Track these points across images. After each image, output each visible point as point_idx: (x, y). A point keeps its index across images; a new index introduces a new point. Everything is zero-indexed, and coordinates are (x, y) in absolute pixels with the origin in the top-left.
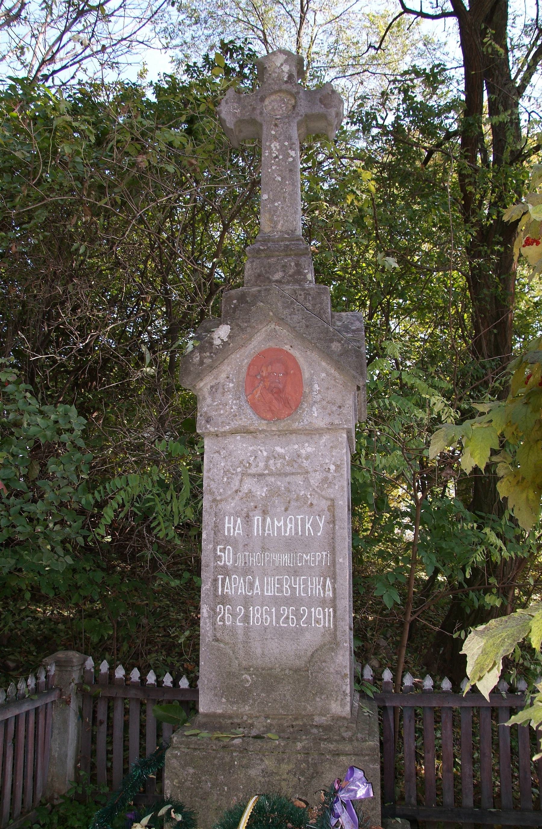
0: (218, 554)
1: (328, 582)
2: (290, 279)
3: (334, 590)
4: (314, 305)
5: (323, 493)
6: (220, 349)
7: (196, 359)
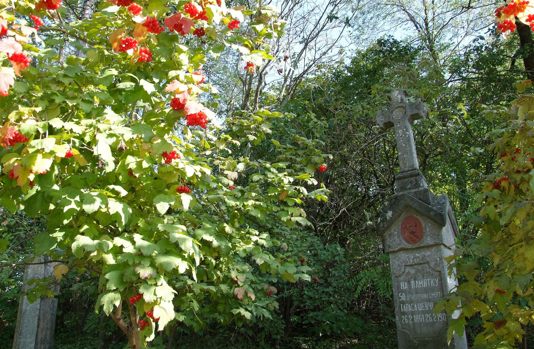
4: (424, 197)
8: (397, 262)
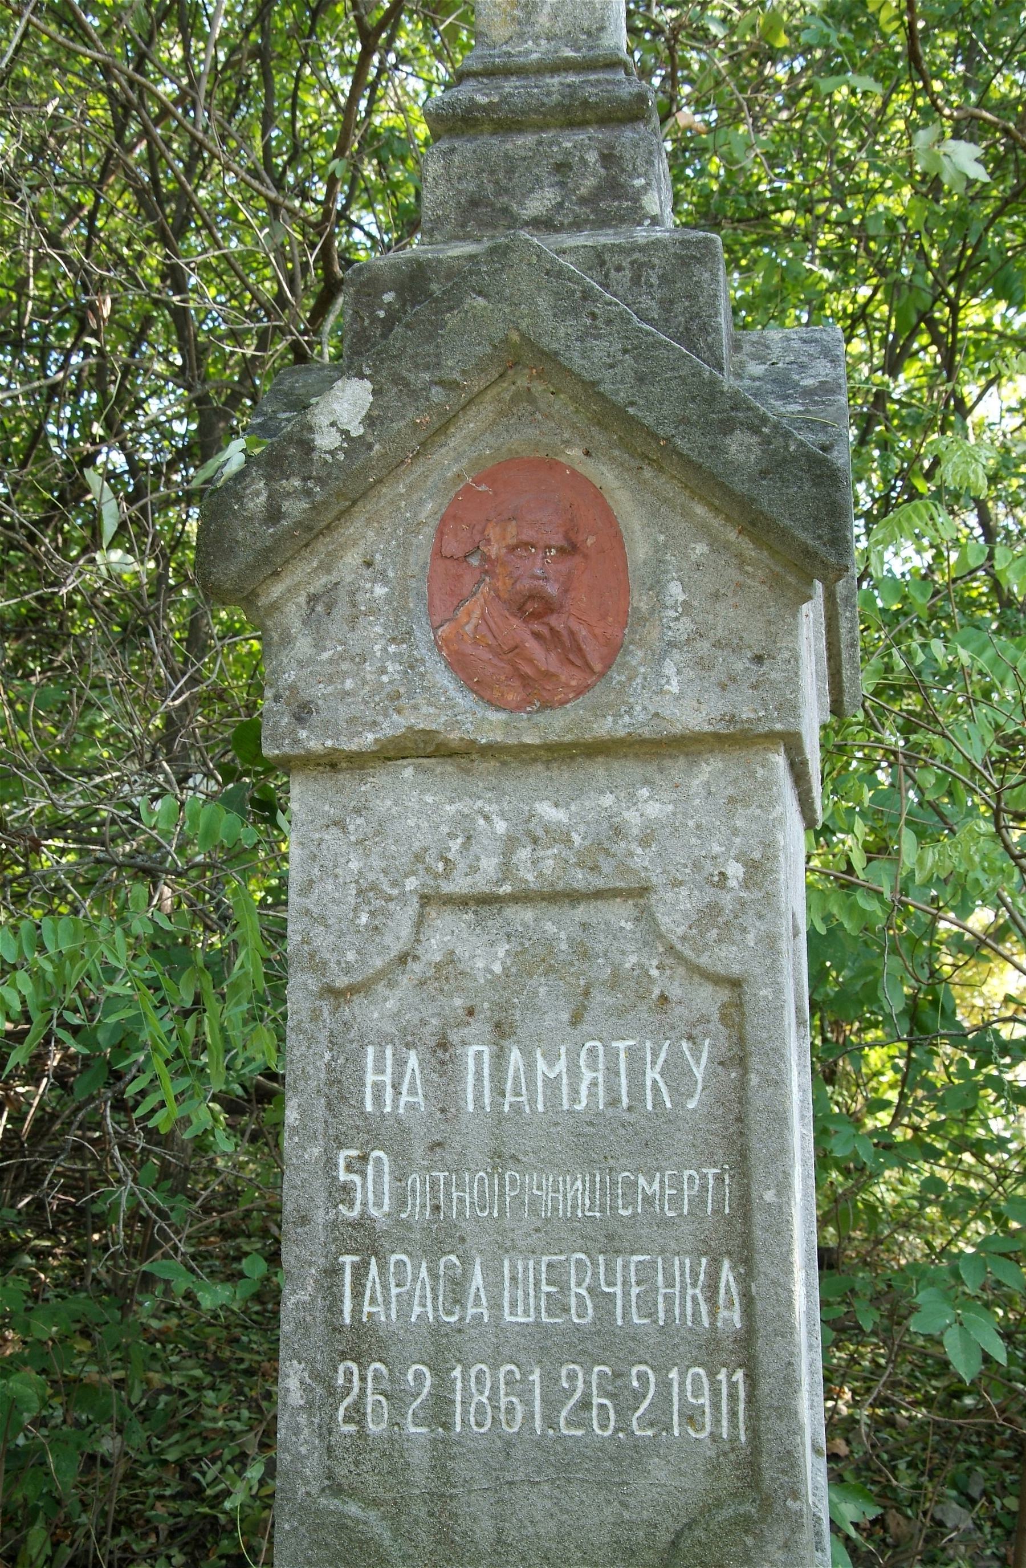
0: (337, 1182)
1: (727, 1274)
2: (582, 211)
3: (748, 1301)
4: (667, 305)
5: (704, 960)
6: (337, 464)
7: (257, 502)
8: (345, 860)
